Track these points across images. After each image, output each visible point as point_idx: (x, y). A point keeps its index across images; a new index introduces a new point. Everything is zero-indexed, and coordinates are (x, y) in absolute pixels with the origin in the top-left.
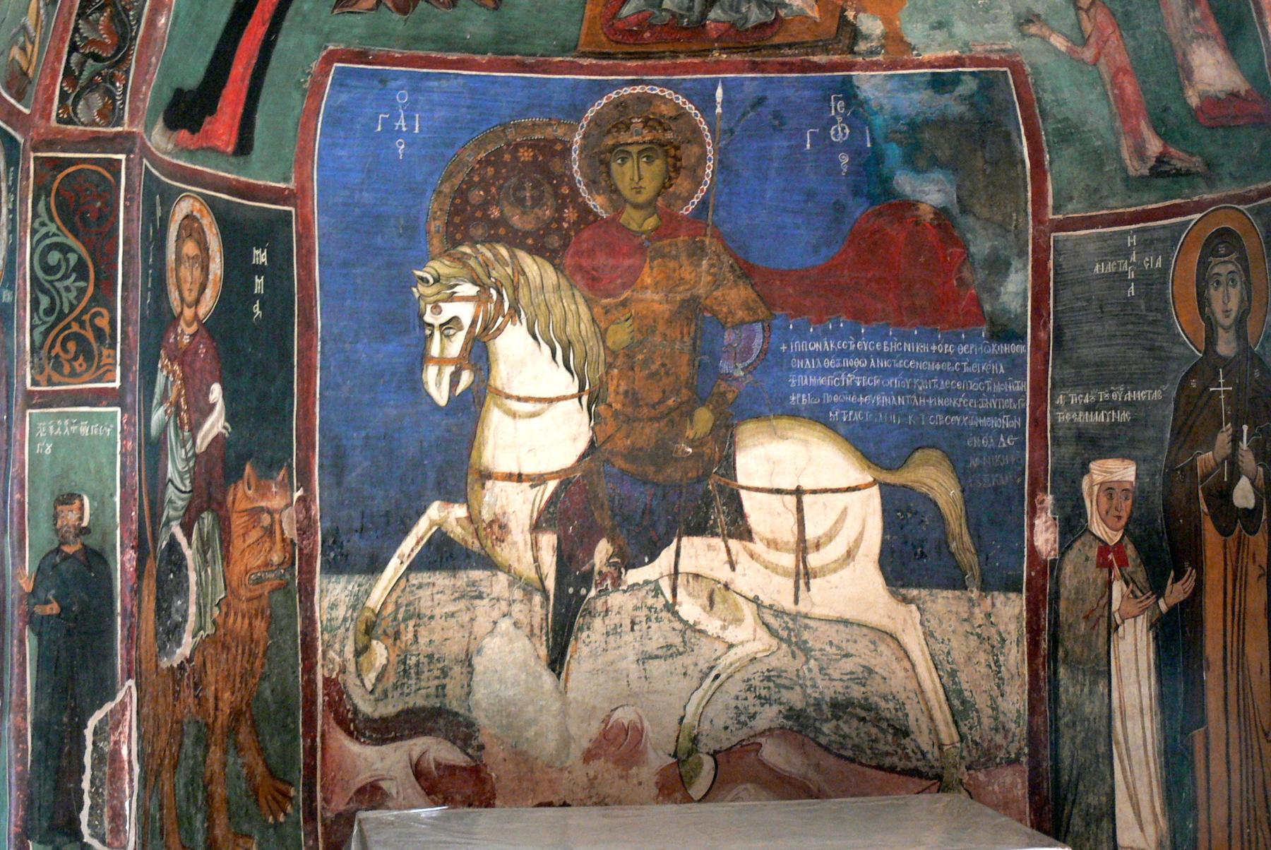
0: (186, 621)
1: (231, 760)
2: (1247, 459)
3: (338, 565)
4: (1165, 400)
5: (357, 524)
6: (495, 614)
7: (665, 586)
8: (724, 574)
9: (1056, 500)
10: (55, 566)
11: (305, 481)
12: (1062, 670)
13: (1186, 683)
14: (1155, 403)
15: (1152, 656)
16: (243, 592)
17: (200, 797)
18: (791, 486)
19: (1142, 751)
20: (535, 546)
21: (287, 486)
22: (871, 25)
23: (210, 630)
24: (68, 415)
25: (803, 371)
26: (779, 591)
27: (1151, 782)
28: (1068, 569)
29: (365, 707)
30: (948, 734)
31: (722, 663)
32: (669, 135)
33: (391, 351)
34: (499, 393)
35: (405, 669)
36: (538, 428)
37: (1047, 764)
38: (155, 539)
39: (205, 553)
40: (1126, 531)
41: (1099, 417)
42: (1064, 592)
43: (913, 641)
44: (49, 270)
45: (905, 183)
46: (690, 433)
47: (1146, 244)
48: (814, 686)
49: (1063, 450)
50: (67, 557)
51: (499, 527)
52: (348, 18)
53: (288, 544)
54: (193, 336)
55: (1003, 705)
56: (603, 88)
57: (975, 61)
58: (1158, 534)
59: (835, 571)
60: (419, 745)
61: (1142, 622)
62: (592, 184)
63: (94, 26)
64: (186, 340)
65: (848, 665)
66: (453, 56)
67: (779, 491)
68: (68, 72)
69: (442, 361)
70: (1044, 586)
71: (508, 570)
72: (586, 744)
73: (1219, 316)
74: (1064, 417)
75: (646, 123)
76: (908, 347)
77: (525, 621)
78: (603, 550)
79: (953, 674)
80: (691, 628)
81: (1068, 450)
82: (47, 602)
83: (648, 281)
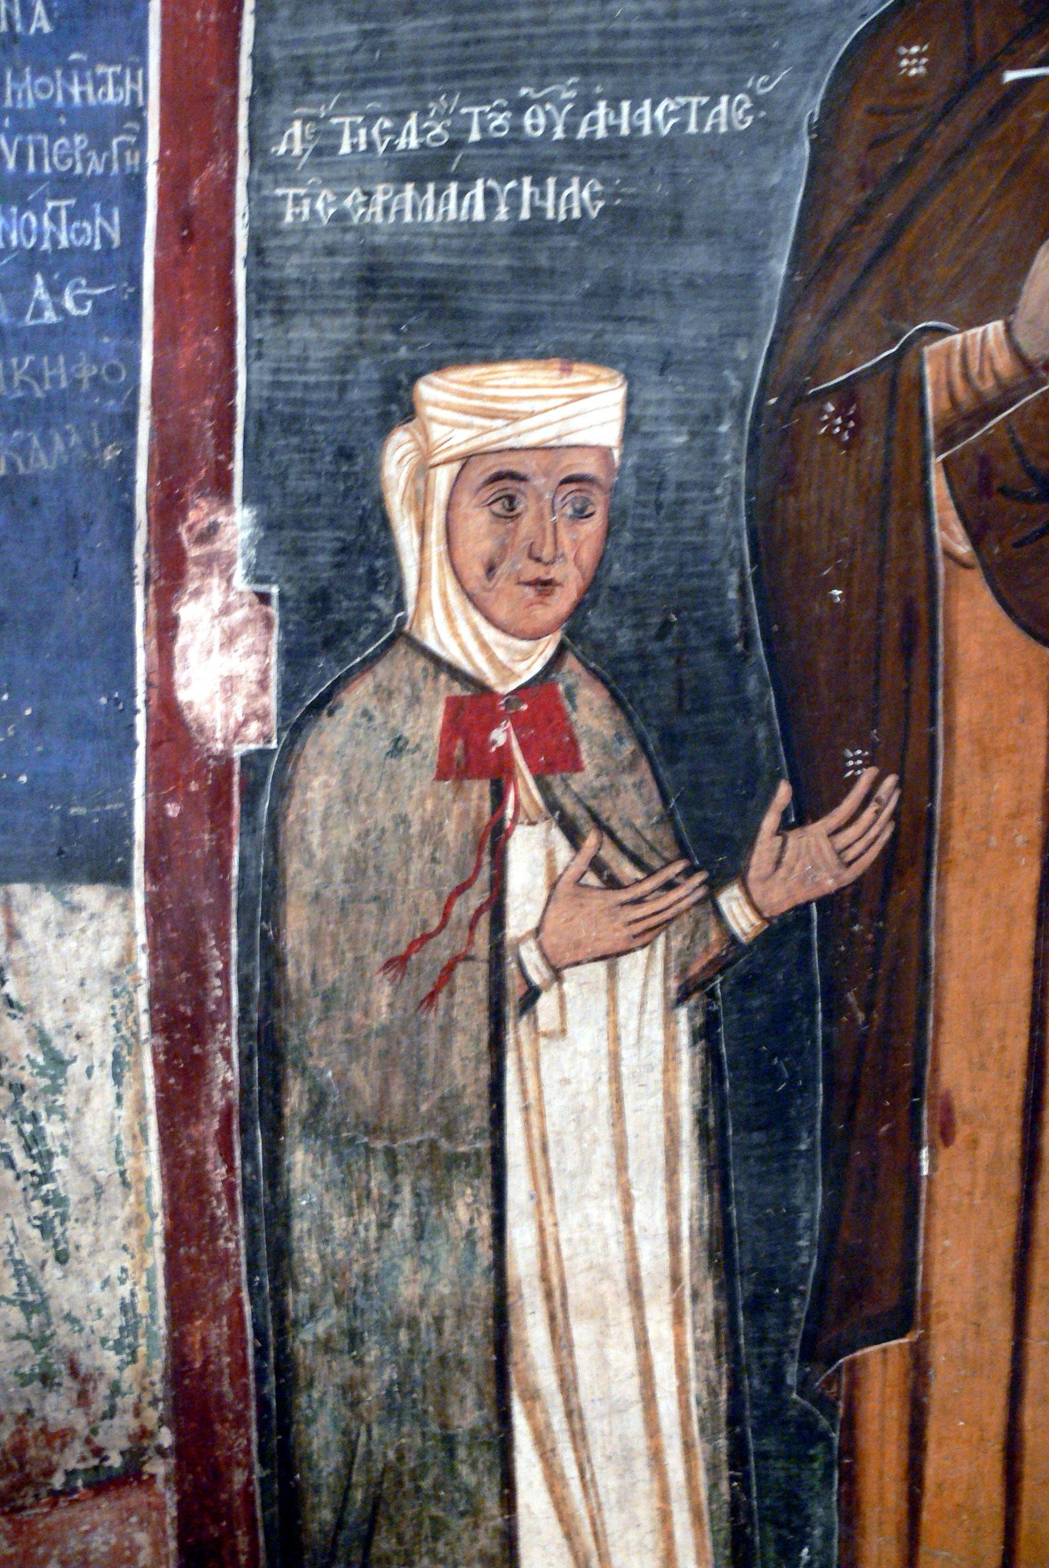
4: (768, 129)
9: (269, 527)
12: (300, 1162)
13: (834, 1183)
14: (718, 149)
15: (686, 1095)
19: (635, 1417)
27: (665, 1517)
28: (316, 788)
37: (246, 1476)
40: (575, 633)
41: (465, 205)
42: (300, 877)
49: (302, 331)
55: (64, 1289)
58: (724, 645)
61: (644, 978)
70: (221, 855)
74: (308, 205)
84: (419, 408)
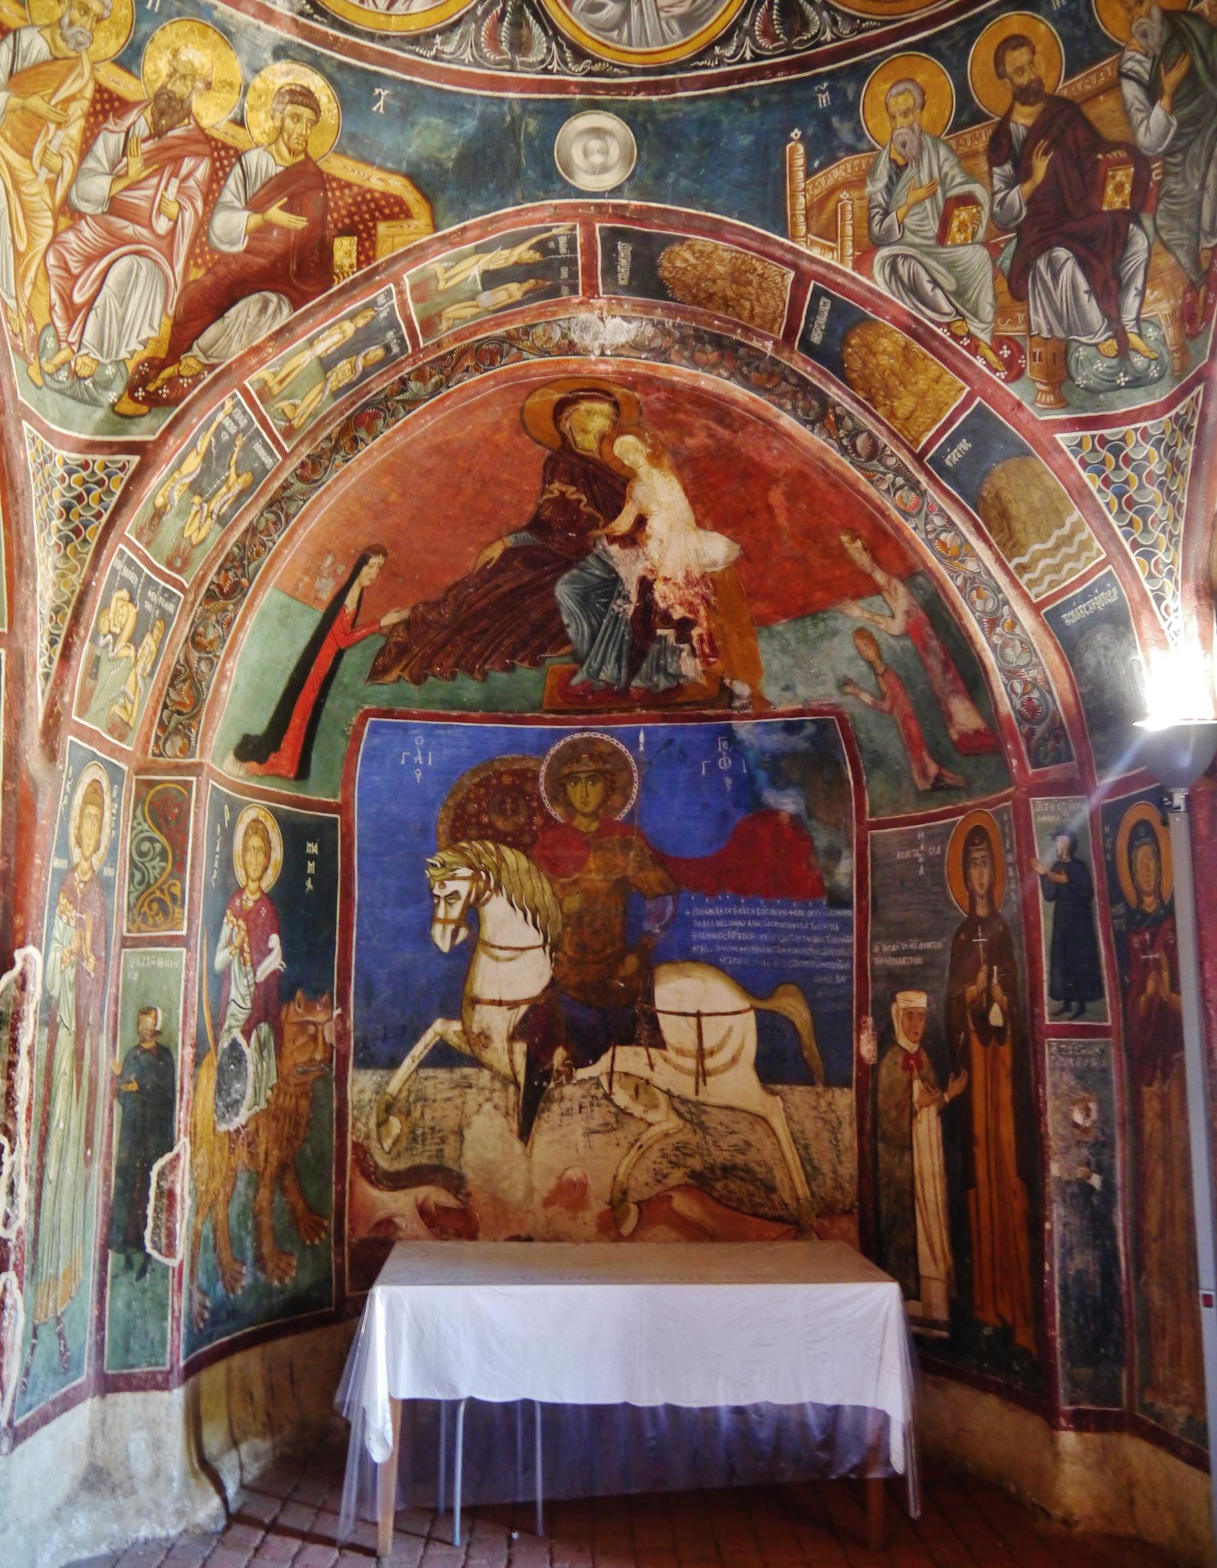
0: (243, 1098)
1: (277, 1198)
2: (997, 991)
3: (365, 1063)
5: (381, 1033)
6: (481, 1099)
7: (604, 1081)
8: (645, 1072)
9: (875, 1021)
10: (136, 1058)
11: (343, 1002)
12: (881, 1146)
14: (938, 951)
16: (292, 1080)
17: (250, 1224)
18: (694, 1011)
20: (511, 1052)
21: (329, 1007)
22: (742, 689)
23: (263, 1105)
24: (150, 953)
25: (701, 929)
26: (685, 1086)
28: (883, 1071)
29: (384, 1163)
30: (803, 1190)
31: (644, 1138)
32: (608, 766)
33: (408, 915)
34: (486, 944)
35: (413, 1137)
36: (515, 969)
38: (216, 1041)
39: (261, 1052)
41: (902, 961)
43: (779, 1123)
44: (142, 855)
45: (771, 798)
46: (622, 973)
47: (931, 838)
48: (710, 1154)
50: (145, 1051)
51: (484, 1038)
52: (377, 688)
53: (328, 1048)
54: (256, 902)
56: (560, 735)
57: (813, 712)
59: (723, 1071)
60: (422, 1192)
61: (933, 1110)
62: (554, 800)
63: (179, 692)
64: (250, 904)
65: (733, 1140)
66: (455, 713)
67: (685, 1014)
68: (161, 722)
69: (446, 922)
71: (490, 1068)
72: (545, 1194)
73: (977, 888)
74: (879, 961)
75: (591, 757)
76: (774, 912)
77: (502, 1104)
78: (560, 1055)
79: (806, 1147)
80: (622, 1113)
81: (881, 985)
82: (130, 1082)
83: (592, 866)
84: (701, 532)
